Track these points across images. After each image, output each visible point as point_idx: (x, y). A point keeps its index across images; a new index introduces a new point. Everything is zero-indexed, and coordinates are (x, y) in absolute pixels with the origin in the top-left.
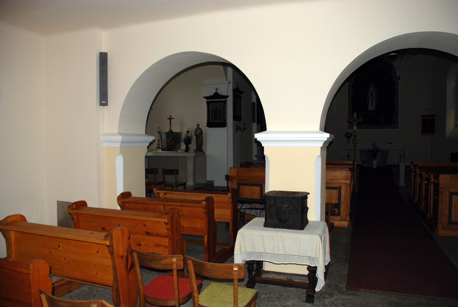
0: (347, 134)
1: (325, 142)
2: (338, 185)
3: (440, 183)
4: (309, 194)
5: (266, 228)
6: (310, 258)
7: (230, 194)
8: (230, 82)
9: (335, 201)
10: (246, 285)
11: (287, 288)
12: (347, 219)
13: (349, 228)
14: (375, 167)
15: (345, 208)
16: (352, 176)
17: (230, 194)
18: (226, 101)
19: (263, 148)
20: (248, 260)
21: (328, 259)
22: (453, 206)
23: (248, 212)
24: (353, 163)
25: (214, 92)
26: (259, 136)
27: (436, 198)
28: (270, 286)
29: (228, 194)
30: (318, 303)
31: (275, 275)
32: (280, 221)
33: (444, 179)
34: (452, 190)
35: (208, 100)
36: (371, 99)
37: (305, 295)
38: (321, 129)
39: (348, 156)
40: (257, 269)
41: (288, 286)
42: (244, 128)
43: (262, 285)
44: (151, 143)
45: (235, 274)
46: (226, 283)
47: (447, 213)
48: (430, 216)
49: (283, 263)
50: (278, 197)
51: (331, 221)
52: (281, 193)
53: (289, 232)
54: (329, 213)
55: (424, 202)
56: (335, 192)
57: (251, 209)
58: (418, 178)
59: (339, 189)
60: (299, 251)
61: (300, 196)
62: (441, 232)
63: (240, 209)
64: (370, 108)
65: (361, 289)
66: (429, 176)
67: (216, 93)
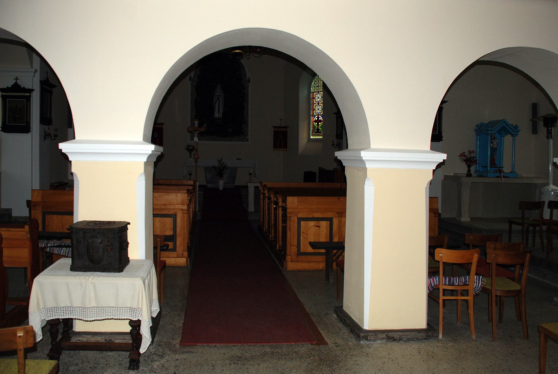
0: (188, 146)
1: (150, 156)
2: (172, 212)
3: (288, 207)
4: (129, 223)
5: (73, 273)
6: (132, 310)
7: (27, 227)
8: (36, 71)
9: (169, 233)
10: (48, 355)
11: (105, 352)
12: (184, 255)
13: (187, 266)
14: (221, 188)
15: (182, 242)
16: (190, 201)
17: (27, 227)
18: (30, 96)
19: (343, 168)
20: (50, 319)
21: (156, 309)
22: (302, 234)
23: (56, 251)
24: (194, 184)
25: (12, 82)
26: (64, 147)
27: (285, 225)
28: (83, 353)
29: (24, 228)
30: (145, 369)
31: (89, 336)
32: (92, 261)
33: (292, 201)
34: (300, 215)
35: (4, 94)
36: (217, 103)
37: (128, 360)
38: (145, 139)
39: (190, 174)
40: (64, 331)
41: (106, 350)
42: (56, 136)
43: (72, 352)
44: (439, 166)
45: (19, 340)
46: (98, 352)
47: (296, 243)
48: (279, 247)
49: (96, 319)
50: (89, 229)
51: (162, 259)
52: (92, 224)
53: (103, 276)
54: (159, 248)
55: (273, 232)
56: (169, 221)
57: (60, 246)
58: (267, 201)
59: (174, 216)
60: (117, 301)
61: (117, 226)
62: (291, 266)
63: (45, 248)
64: (217, 115)
65: (199, 344)
66: (277, 199)
67: (16, 84)
